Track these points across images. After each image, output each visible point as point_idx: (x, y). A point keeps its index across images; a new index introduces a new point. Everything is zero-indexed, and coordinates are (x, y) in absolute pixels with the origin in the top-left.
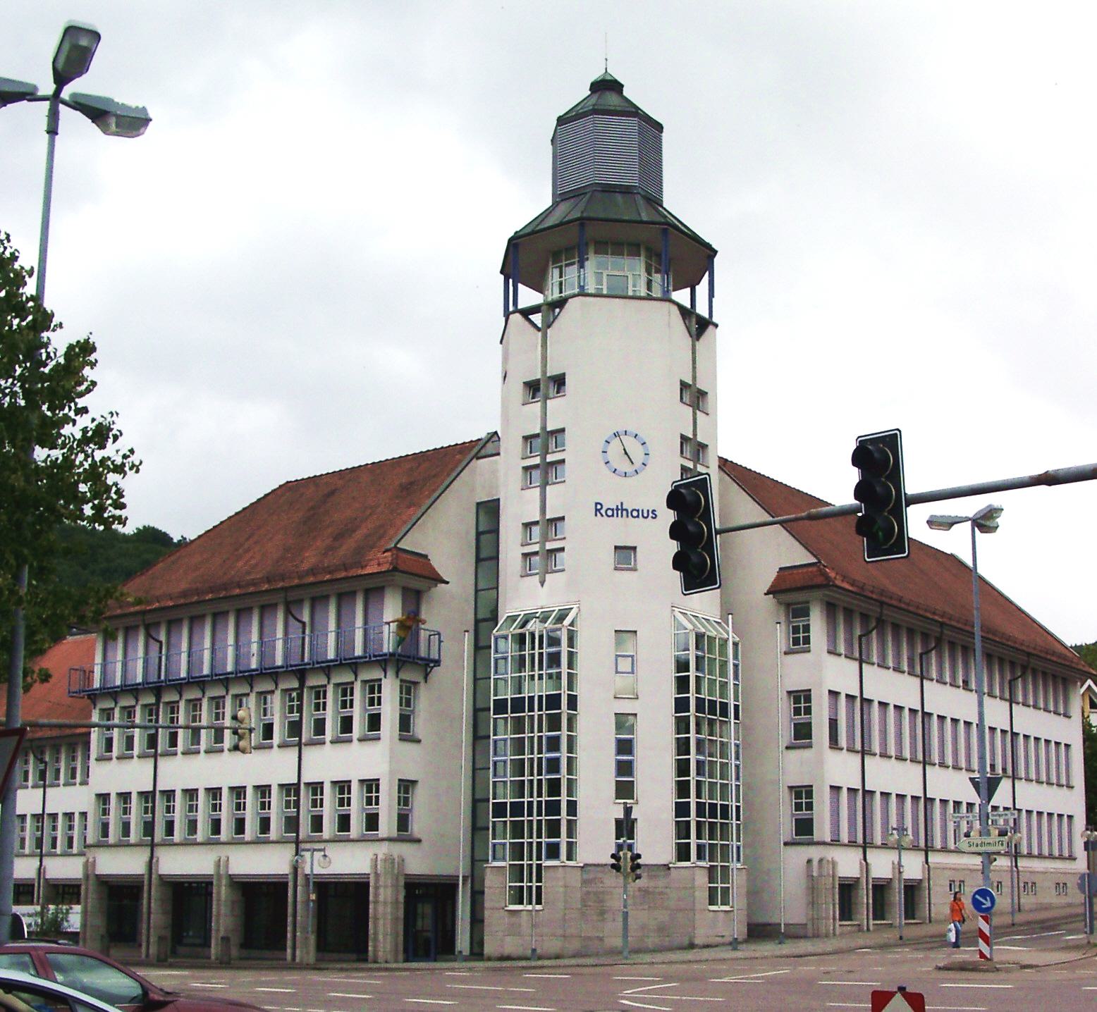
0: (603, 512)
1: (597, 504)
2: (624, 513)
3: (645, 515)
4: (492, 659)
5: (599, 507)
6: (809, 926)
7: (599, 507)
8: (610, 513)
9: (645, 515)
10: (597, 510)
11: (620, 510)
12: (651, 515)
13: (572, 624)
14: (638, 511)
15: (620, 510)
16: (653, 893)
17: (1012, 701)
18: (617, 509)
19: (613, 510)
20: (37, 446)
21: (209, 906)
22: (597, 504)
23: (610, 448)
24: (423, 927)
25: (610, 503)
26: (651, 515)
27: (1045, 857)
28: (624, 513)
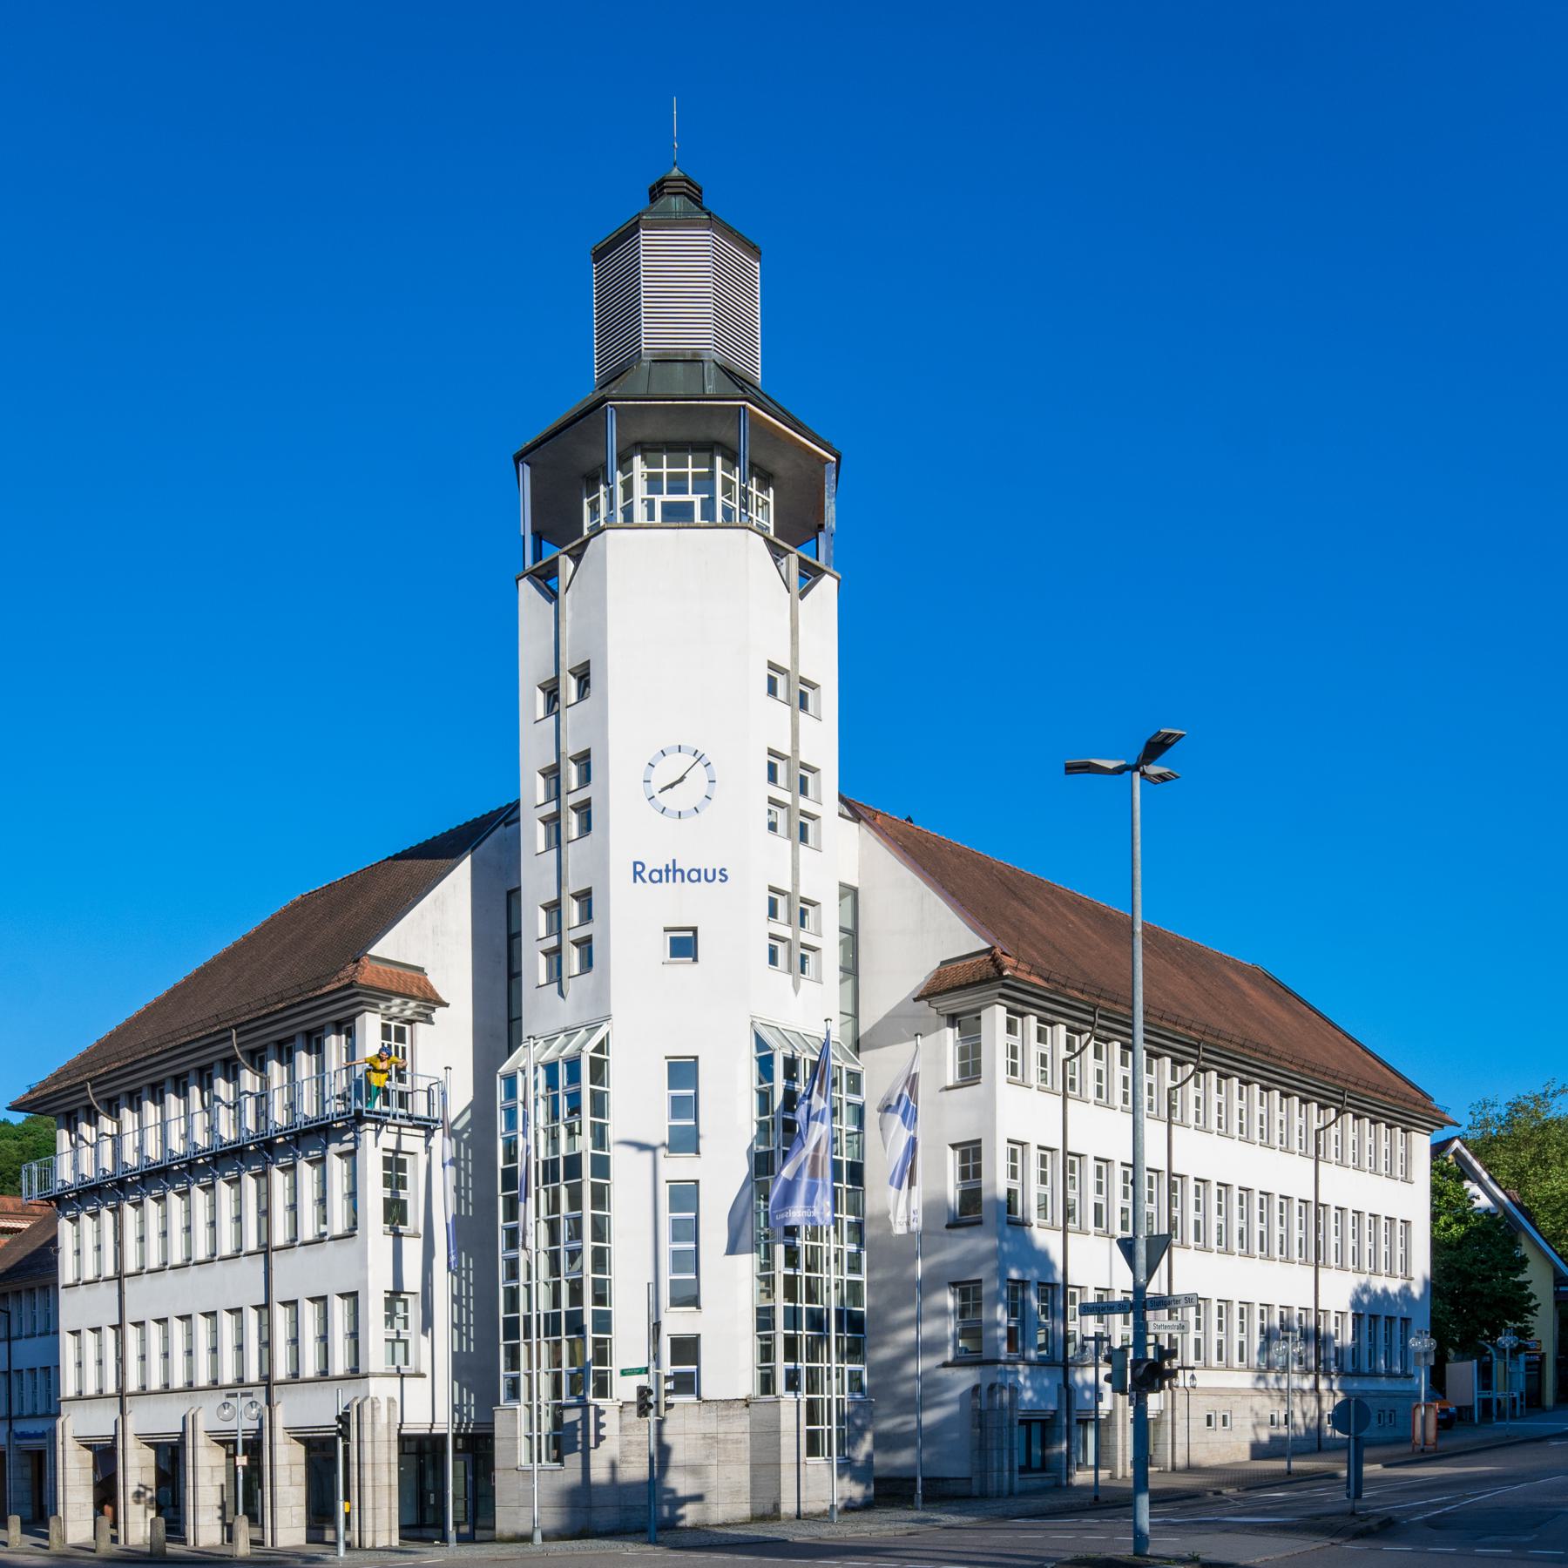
0: (645, 875)
1: (635, 863)
2: (679, 875)
3: (710, 877)
4: (501, 1200)
5: (639, 868)
6: (975, 1483)
7: (639, 868)
8: (656, 876)
9: (710, 877)
10: (636, 873)
11: (671, 872)
12: (718, 876)
13: (600, 1048)
14: (699, 871)
15: (671, 872)
16: (726, 1441)
17: (1068, 1088)
18: (667, 871)
19: (660, 872)
20: (385, 948)
21: (46, 1501)
22: (635, 863)
23: (674, 757)
24: (374, 1541)
25: (654, 861)
26: (718, 876)
27: (1365, 1375)
28: (679, 875)
